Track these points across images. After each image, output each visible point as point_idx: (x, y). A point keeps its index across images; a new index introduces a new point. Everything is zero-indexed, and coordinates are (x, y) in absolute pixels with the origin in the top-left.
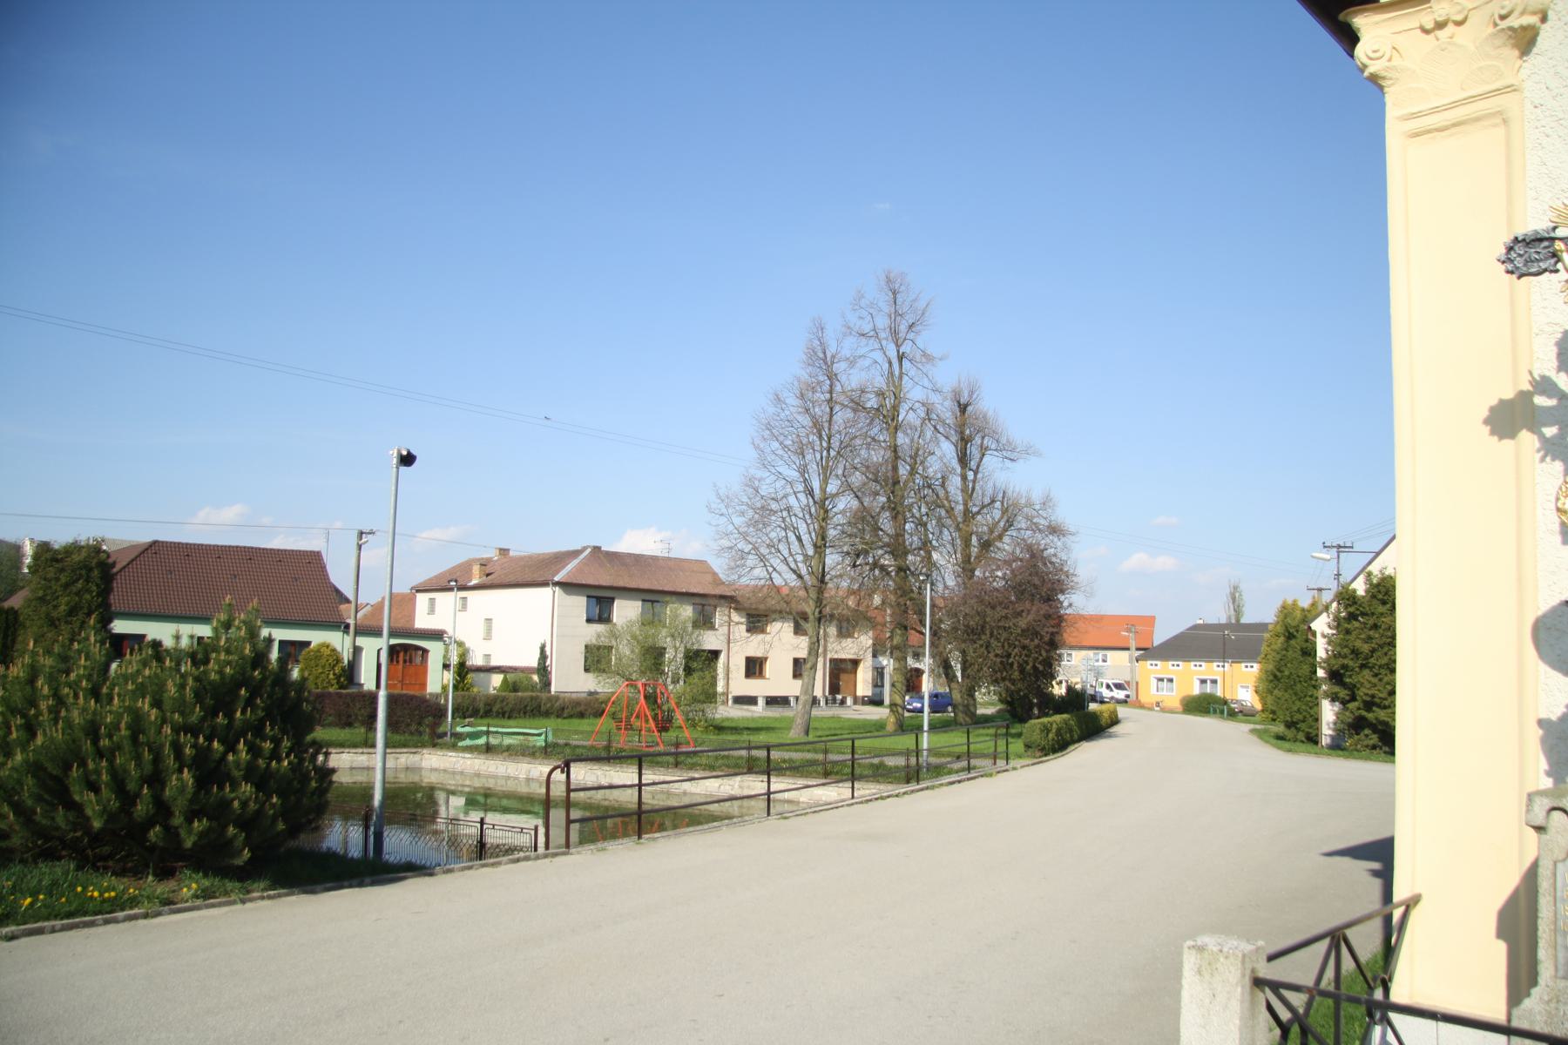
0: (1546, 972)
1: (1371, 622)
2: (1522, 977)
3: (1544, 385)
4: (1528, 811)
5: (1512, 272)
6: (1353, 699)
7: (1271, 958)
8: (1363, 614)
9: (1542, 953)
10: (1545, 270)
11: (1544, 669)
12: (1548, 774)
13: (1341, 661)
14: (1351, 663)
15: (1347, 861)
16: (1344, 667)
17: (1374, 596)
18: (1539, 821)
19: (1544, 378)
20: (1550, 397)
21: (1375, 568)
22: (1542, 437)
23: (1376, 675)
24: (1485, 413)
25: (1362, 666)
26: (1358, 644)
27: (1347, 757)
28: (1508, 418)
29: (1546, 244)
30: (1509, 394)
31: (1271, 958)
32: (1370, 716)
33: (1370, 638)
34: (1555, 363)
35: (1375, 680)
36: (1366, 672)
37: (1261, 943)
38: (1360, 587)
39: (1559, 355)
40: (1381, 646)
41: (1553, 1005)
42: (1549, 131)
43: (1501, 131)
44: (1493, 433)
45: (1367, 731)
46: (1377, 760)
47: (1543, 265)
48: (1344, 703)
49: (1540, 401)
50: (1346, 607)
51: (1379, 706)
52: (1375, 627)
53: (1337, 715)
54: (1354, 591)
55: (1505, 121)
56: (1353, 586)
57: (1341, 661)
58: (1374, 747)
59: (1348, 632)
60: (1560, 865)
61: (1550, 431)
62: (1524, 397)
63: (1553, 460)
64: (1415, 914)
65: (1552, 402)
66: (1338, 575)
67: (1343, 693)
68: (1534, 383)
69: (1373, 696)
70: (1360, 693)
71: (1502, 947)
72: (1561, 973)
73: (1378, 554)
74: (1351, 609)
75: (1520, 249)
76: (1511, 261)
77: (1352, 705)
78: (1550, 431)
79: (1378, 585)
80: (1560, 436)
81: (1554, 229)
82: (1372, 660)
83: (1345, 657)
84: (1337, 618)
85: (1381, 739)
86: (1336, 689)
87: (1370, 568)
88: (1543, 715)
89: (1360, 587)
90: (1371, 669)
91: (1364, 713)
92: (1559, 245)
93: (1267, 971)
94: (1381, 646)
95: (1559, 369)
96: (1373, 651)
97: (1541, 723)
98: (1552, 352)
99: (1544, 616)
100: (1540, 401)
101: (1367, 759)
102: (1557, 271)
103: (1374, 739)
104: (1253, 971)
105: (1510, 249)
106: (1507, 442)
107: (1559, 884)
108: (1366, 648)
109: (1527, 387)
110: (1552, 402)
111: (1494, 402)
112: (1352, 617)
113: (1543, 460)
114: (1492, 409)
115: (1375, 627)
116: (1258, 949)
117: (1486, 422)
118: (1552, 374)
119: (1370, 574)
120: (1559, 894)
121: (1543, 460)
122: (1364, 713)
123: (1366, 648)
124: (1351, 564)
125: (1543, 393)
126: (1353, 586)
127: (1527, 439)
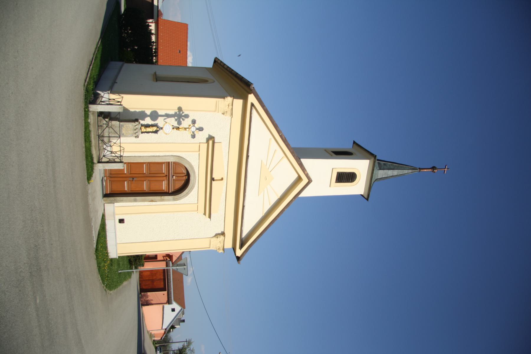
28: (180, 109)
78: (176, 118)
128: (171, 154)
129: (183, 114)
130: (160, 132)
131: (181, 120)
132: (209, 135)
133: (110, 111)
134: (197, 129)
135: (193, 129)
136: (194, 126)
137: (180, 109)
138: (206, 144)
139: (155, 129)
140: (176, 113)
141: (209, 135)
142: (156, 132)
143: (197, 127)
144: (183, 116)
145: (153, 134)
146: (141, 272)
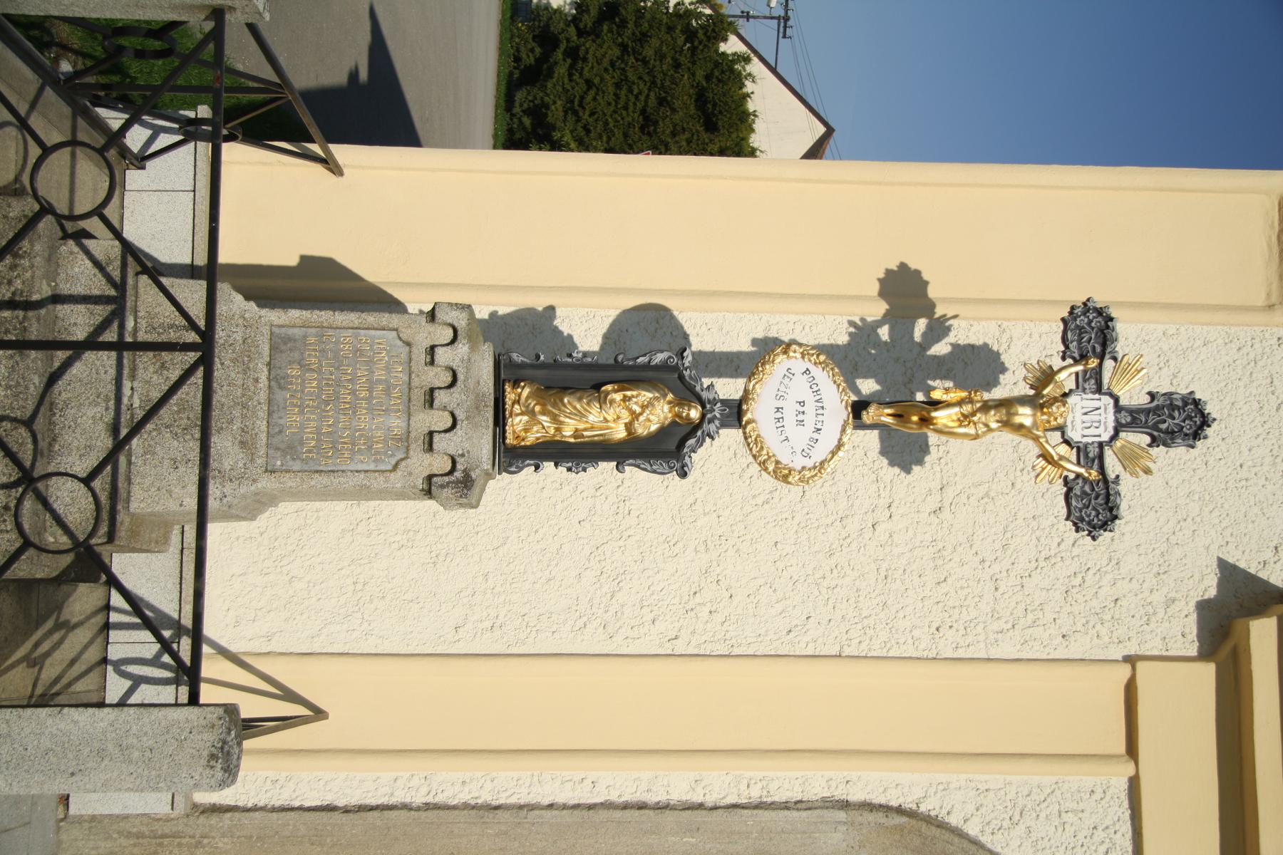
0: (275, 316)
1: (682, 59)
2: (267, 286)
3: (939, 329)
4: (450, 304)
5: (1071, 313)
6: (580, 33)
7: (252, 28)
8: (693, 50)
9: (294, 314)
10: (1067, 347)
11: (613, 314)
12: (493, 315)
13: (631, 19)
14: (628, 32)
15: (365, 38)
16: (623, 24)
17: (717, 64)
18: (440, 315)
19: (949, 329)
20: (924, 335)
21: (756, 67)
22: (879, 324)
23: (612, 64)
24: (913, 265)
25: (624, 47)
26: (655, 42)
27: (502, 23)
28: (904, 289)
29: (1098, 349)
30: (932, 292)
31: (252, 28)
32: (559, 54)
33: (662, 57)
34: (962, 341)
35: (606, 63)
36: (616, 52)
37: (267, 16)
38: (732, 46)
39: (972, 346)
40: (650, 73)
41: (241, 321)
42: (1245, 351)
43: (1261, 301)
44: (889, 272)
45: (538, 50)
46: (500, 64)
47: (1073, 346)
48: (575, 20)
49: (921, 325)
50: (702, 27)
51: (572, 67)
52: (677, 66)
53: (558, 11)
54: (725, 40)
55: (1271, 307)
56: (733, 39)
57: (631, 19)
58: (517, 59)
59: (670, 29)
60: (394, 333)
61: (884, 333)
62: (927, 308)
63: (850, 334)
64: (318, 169)
65: (917, 336)
66: (747, 16)
67: (588, 20)
68: (944, 318)
69: (585, 60)
70: (589, 44)
71: (293, 261)
72: (276, 330)
73: (773, 70)
74: (700, 34)
75: (1097, 322)
76: (1084, 314)
77: (572, 30)
78: (884, 333)
79: (732, 71)
80: (878, 343)
81: (1115, 359)
82: (632, 60)
83: (637, 24)
84: (689, 14)
85: (528, 68)
86: (594, 12)
87: (755, 60)
88: (559, 312)
89: (732, 46)
90: (621, 58)
91: (563, 46)
92: (1093, 363)
93: (234, 21)
94: (650, 73)
95: (955, 346)
96: (645, 62)
97: (551, 310)
98: (976, 339)
99: (672, 317)
100: (921, 325)
101: (502, 51)
102: (1064, 358)
103: (528, 60)
104: (232, 9)
105: (1099, 312)
106: (876, 287)
107: (372, 332)
108: (649, 52)
109: (939, 312)
110: (917, 336)
111: (925, 276)
112: (690, 34)
113: (851, 323)
114: (918, 273)
115: (677, 66)
116: (260, 14)
117: (903, 266)
118: (951, 338)
119: (747, 60)
120: (362, 332)
121: (851, 323)
122: (563, 46)
123: (649, 52)
124: (762, 34)
125: (930, 328)
126: (733, 39)
127: (878, 309)
128: (816, 781)
129: (941, 349)
130: (718, 453)
131: (941, 349)
132: (1228, 571)
133: (191, 281)
134: (1129, 418)
135: (1087, 418)
136: (1094, 382)
137: (904, 289)
138: (1208, 671)
139: (655, 412)
140: (863, 332)
141: (1228, 571)
142: (666, 450)
143: (1133, 394)
144: (942, 368)
145: (636, 477)
146: (678, 415)
